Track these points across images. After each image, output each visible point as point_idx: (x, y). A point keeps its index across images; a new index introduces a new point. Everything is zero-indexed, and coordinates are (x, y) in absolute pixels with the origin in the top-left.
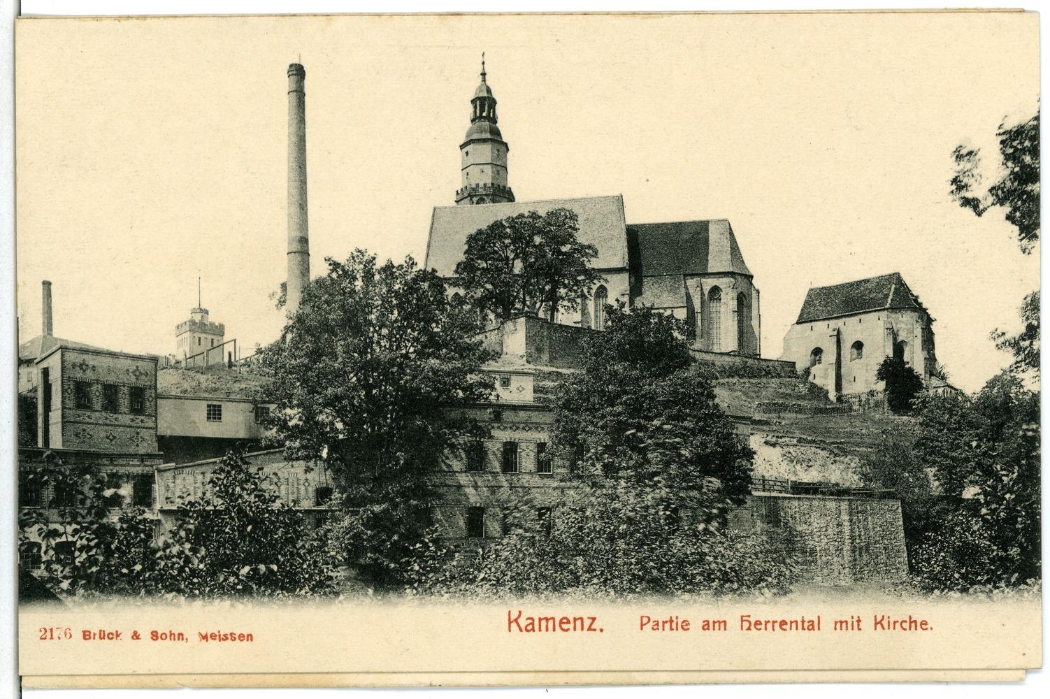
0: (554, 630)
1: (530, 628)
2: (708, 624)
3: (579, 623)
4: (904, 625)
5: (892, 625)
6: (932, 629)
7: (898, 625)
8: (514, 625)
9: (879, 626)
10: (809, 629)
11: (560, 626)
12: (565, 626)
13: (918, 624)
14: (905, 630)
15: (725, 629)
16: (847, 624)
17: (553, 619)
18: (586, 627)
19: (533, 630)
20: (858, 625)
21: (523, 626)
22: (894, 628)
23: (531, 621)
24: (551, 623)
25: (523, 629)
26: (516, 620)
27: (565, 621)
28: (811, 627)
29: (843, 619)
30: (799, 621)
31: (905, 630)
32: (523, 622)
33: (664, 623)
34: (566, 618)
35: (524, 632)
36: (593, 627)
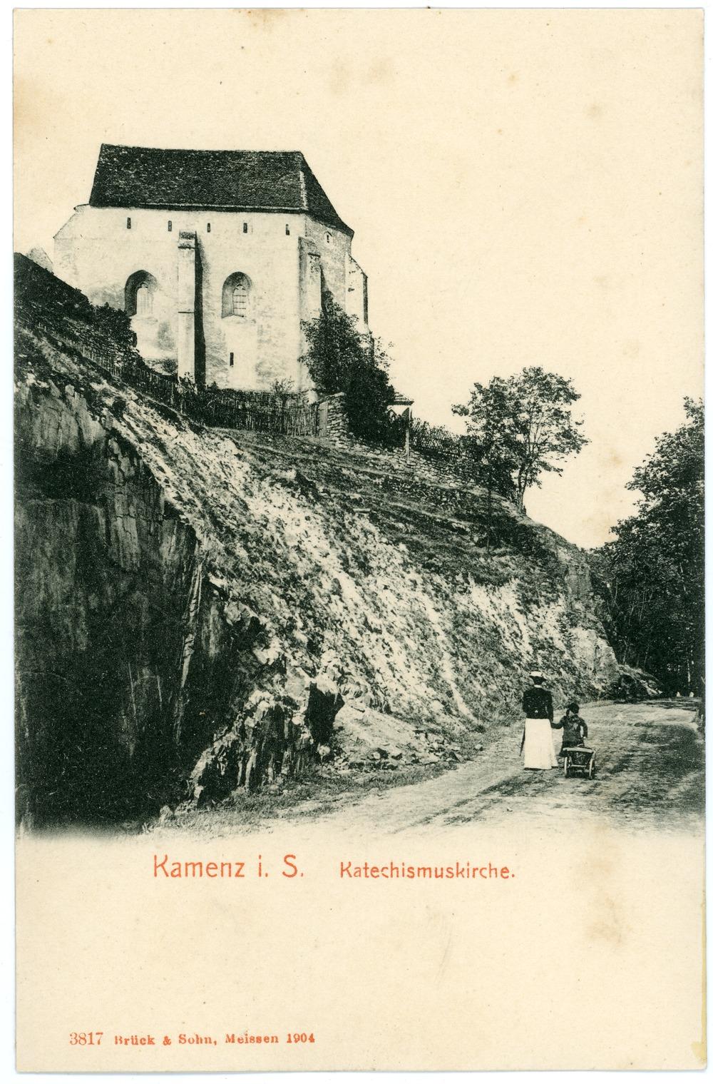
0: (201, 875)
1: (175, 874)
3: (226, 868)
5: (471, 874)
6: (513, 876)
7: (477, 873)
8: (160, 870)
10: (173, 876)
11: (207, 872)
12: (212, 872)
13: (499, 872)
14: (387, 877)
16: (201, 867)
17: (200, 864)
19: (179, 875)
21: (352, 874)
22: (474, 876)
23: (176, 866)
24: (197, 868)
25: (170, 875)
26: (162, 865)
27: (212, 866)
28: (357, 874)
31: (387, 877)
32: (352, 870)
35: (371, 878)
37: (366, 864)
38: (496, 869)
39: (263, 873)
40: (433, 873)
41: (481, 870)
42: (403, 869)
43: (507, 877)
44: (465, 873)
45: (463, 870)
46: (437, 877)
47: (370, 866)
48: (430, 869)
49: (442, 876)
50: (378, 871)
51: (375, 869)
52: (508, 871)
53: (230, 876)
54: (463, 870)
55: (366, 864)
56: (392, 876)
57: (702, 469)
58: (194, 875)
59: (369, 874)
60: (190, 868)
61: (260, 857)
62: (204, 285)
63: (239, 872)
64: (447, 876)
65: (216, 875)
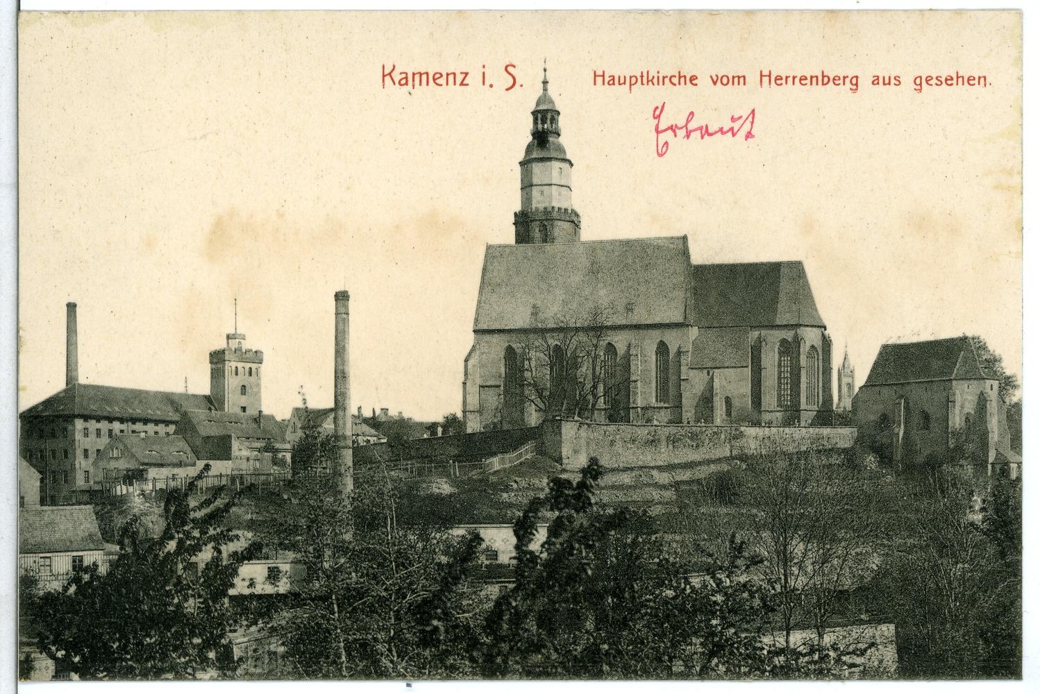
0: (428, 84)
1: (404, 81)
2: (613, 79)
3: (451, 77)
7: (667, 80)
8: (388, 79)
11: (946, 83)
14: (674, 85)
15: (744, 84)
16: (921, 79)
19: (878, 83)
23: (404, 76)
25: (397, 82)
26: (390, 74)
27: (437, 76)
28: (611, 82)
29: (814, 75)
30: (639, 76)
31: (674, 85)
32: (397, 77)
34: (694, 76)
36: (465, 82)
39: (487, 83)
41: (671, 77)
43: (839, 84)
44: (655, 81)
45: (653, 77)
49: (889, 84)
51: (778, 78)
54: (653, 77)
56: (679, 84)
57: (87, 672)
58: (817, 84)
60: (417, 77)
61: (484, 67)
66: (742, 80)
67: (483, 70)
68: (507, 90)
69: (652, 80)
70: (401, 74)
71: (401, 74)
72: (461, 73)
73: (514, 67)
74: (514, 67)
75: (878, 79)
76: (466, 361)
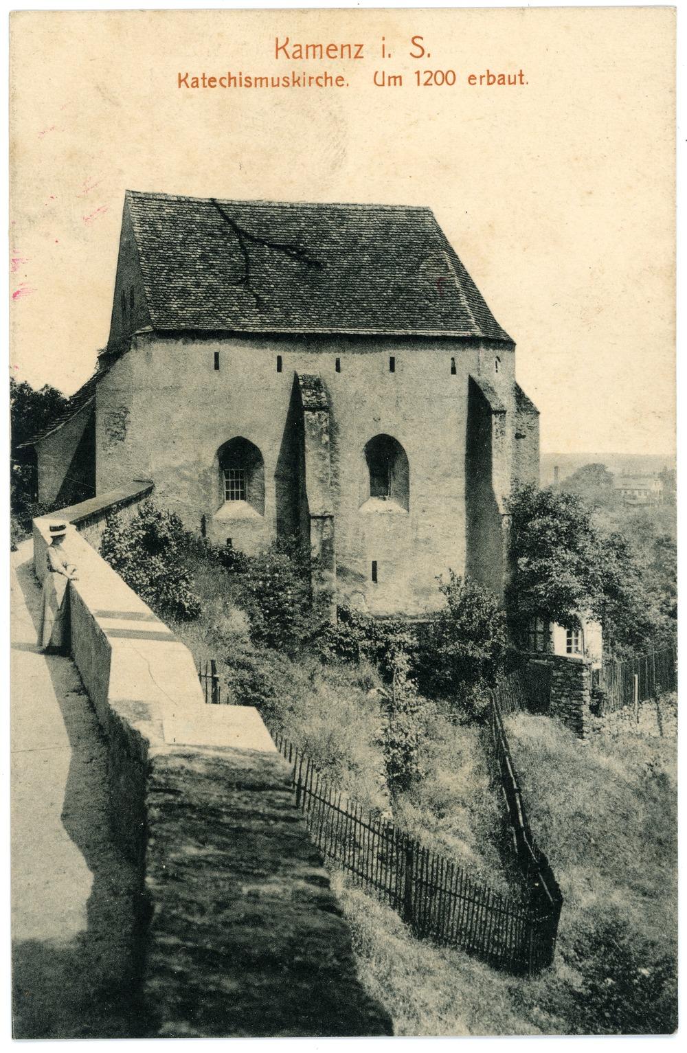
3: (346, 50)
4: (320, 80)
7: (313, 81)
8: (281, 52)
9: (183, 83)
10: (294, 57)
12: (213, 84)
14: (225, 87)
15: (401, 84)
18: (353, 55)
20: (521, 80)
23: (298, 48)
24: (318, 49)
26: (283, 48)
27: (332, 48)
28: (195, 85)
31: (321, 86)
32: (189, 81)
33: (481, 77)
34: (473, 76)
36: (359, 55)
37: (204, 74)
38: (331, 78)
40: (270, 81)
42: (241, 78)
44: (301, 82)
46: (273, 86)
47: (208, 76)
48: (266, 78)
49: (278, 85)
50: (215, 81)
51: (213, 79)
52: (343, 80)
53: (314, 57)
55: (204, 74)
59: (206, 84)
61: (384, 39)
62: (39, 627)
63: (357, 53)
64: (246, 85)
65: (336, 57)
66: (398, 80)
67: (382, 42)
68: (411, 54)
69: (297, 81)
70: (295, 46)
71: (295, 46)
72: (356, 45)
73: (422, 38)
74: (422, 38)
75: (504, 78)
76: (454, 75)
